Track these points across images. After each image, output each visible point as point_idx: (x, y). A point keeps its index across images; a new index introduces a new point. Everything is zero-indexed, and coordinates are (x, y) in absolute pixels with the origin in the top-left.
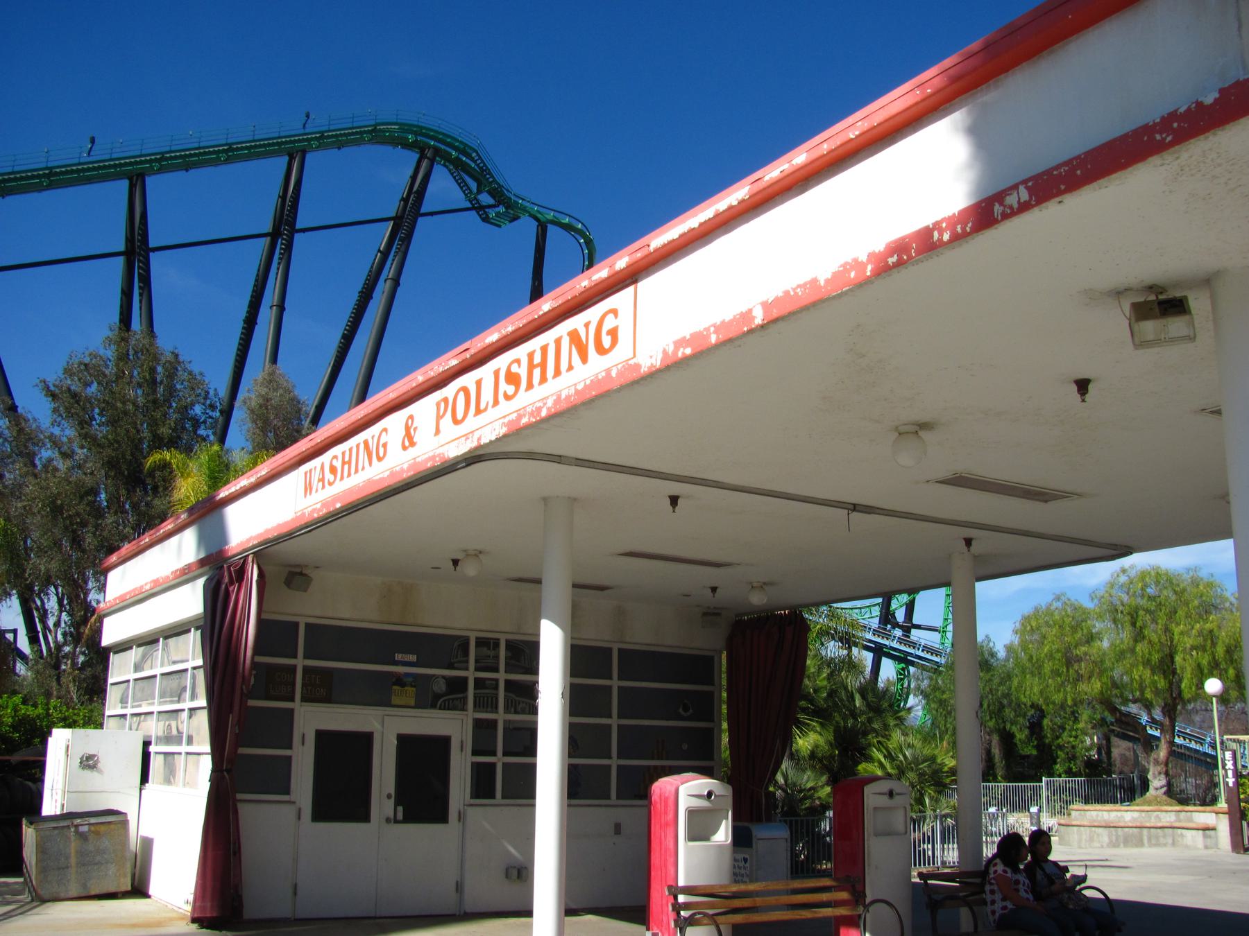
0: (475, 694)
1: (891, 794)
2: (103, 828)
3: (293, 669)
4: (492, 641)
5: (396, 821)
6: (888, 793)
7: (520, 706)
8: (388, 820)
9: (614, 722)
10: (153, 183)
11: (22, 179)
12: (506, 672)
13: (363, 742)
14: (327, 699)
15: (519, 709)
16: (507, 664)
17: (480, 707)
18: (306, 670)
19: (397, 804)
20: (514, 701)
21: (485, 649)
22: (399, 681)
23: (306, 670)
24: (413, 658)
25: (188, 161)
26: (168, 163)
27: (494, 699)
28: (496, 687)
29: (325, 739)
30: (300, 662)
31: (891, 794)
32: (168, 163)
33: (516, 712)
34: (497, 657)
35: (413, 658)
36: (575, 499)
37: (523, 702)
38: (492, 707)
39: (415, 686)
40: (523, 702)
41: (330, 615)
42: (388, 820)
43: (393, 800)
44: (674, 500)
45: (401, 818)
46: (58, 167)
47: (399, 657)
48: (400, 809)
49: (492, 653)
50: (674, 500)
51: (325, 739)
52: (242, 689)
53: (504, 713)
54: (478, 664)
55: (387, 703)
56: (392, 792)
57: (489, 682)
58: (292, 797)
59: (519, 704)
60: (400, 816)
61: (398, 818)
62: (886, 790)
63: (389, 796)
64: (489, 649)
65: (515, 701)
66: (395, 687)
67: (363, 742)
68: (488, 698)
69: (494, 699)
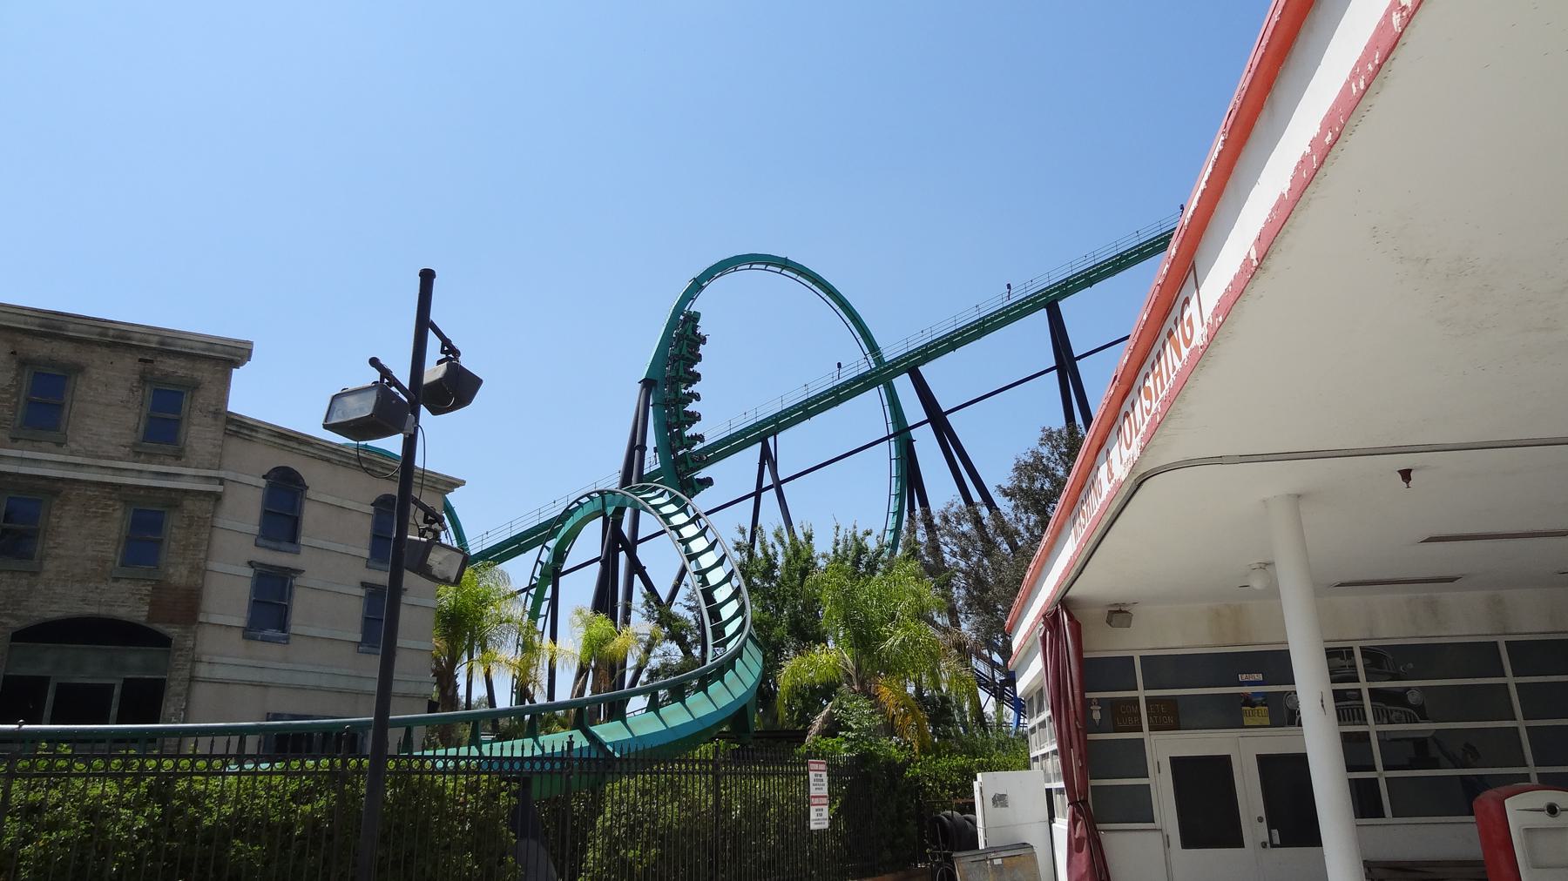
0: (1336, 707)
1: (1552, 810)
2: (1014, 860)
3: (1136, 701)
4: (1344, 650)
5: (1273, 846)
6: (1546, 808)
7: (1394, 715)
8: (1264, 845)
9: (1520, 723)
10: (1064, 305)
11: (964, 332)
12: (1367, 681)
13: (1220, 767)
14: (1176, 727)
15: (1393, 717)
16: (1366, 672)
17: (1345, 720)
18: (1149, 700)
19: (1270, 827)
20: (1385, 711)
21: (1338, 659)
22: (1248, 701)
23: (1149, 700)
24: (1259, 677)
25: (1088, 278)
26: (1070, 286)
27: (1360, 710)
28: (1360, 698)
29: (1182, 767)
30: (1142, 694)
31: (1552, 810)
32: (1070, 286)
33: (1390, 722)
34: (1354, 666)
35: (1259, 677)
36: (1299, 496)
37: (1396, 711)
38: (1360, 719)
39: (1265, 705)
40: (1396, 711)
41: (1160, 646)
42: (1264, 845)
43: (1265, 823)
44: (1406, 475)
45: (1279, 843)
46: (988, 316)
47: (1243, 677)
48: (1275, 832)
49: (1347, 663)
50: (1406, 475)
51: (1182, 767)
52: (1076, 725)
53: (1376, 724)
54: (1333, 676)
55: (1241, 725)
56: (1262, 813)
57: (1351, 693)
58: (1157, 825)
59: (1392, 713)
60: (1277, 840)
61: (1275, 843)
62: (1543, 805)
63: (1260, 820)
64: (1343, 659)
65: (1387, 712)
66: (1244, 708)
67: (1220, 767)
68: (1352, 710)
69: (1360, 710)
